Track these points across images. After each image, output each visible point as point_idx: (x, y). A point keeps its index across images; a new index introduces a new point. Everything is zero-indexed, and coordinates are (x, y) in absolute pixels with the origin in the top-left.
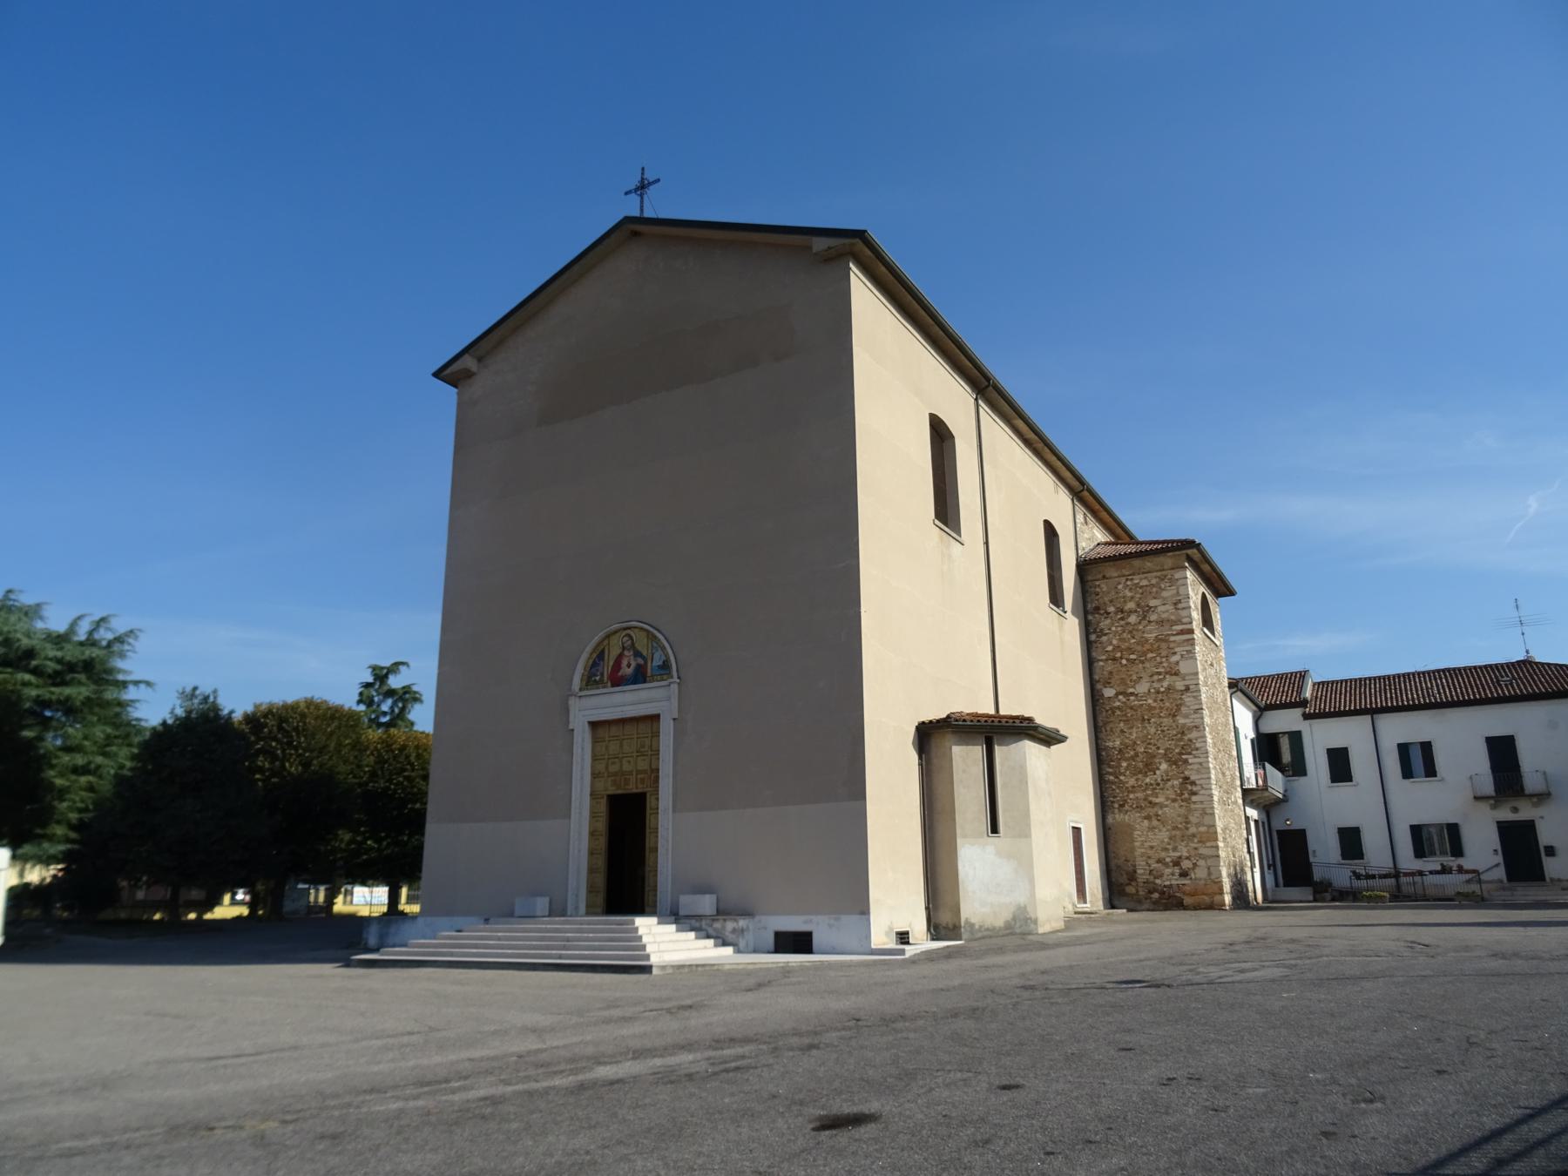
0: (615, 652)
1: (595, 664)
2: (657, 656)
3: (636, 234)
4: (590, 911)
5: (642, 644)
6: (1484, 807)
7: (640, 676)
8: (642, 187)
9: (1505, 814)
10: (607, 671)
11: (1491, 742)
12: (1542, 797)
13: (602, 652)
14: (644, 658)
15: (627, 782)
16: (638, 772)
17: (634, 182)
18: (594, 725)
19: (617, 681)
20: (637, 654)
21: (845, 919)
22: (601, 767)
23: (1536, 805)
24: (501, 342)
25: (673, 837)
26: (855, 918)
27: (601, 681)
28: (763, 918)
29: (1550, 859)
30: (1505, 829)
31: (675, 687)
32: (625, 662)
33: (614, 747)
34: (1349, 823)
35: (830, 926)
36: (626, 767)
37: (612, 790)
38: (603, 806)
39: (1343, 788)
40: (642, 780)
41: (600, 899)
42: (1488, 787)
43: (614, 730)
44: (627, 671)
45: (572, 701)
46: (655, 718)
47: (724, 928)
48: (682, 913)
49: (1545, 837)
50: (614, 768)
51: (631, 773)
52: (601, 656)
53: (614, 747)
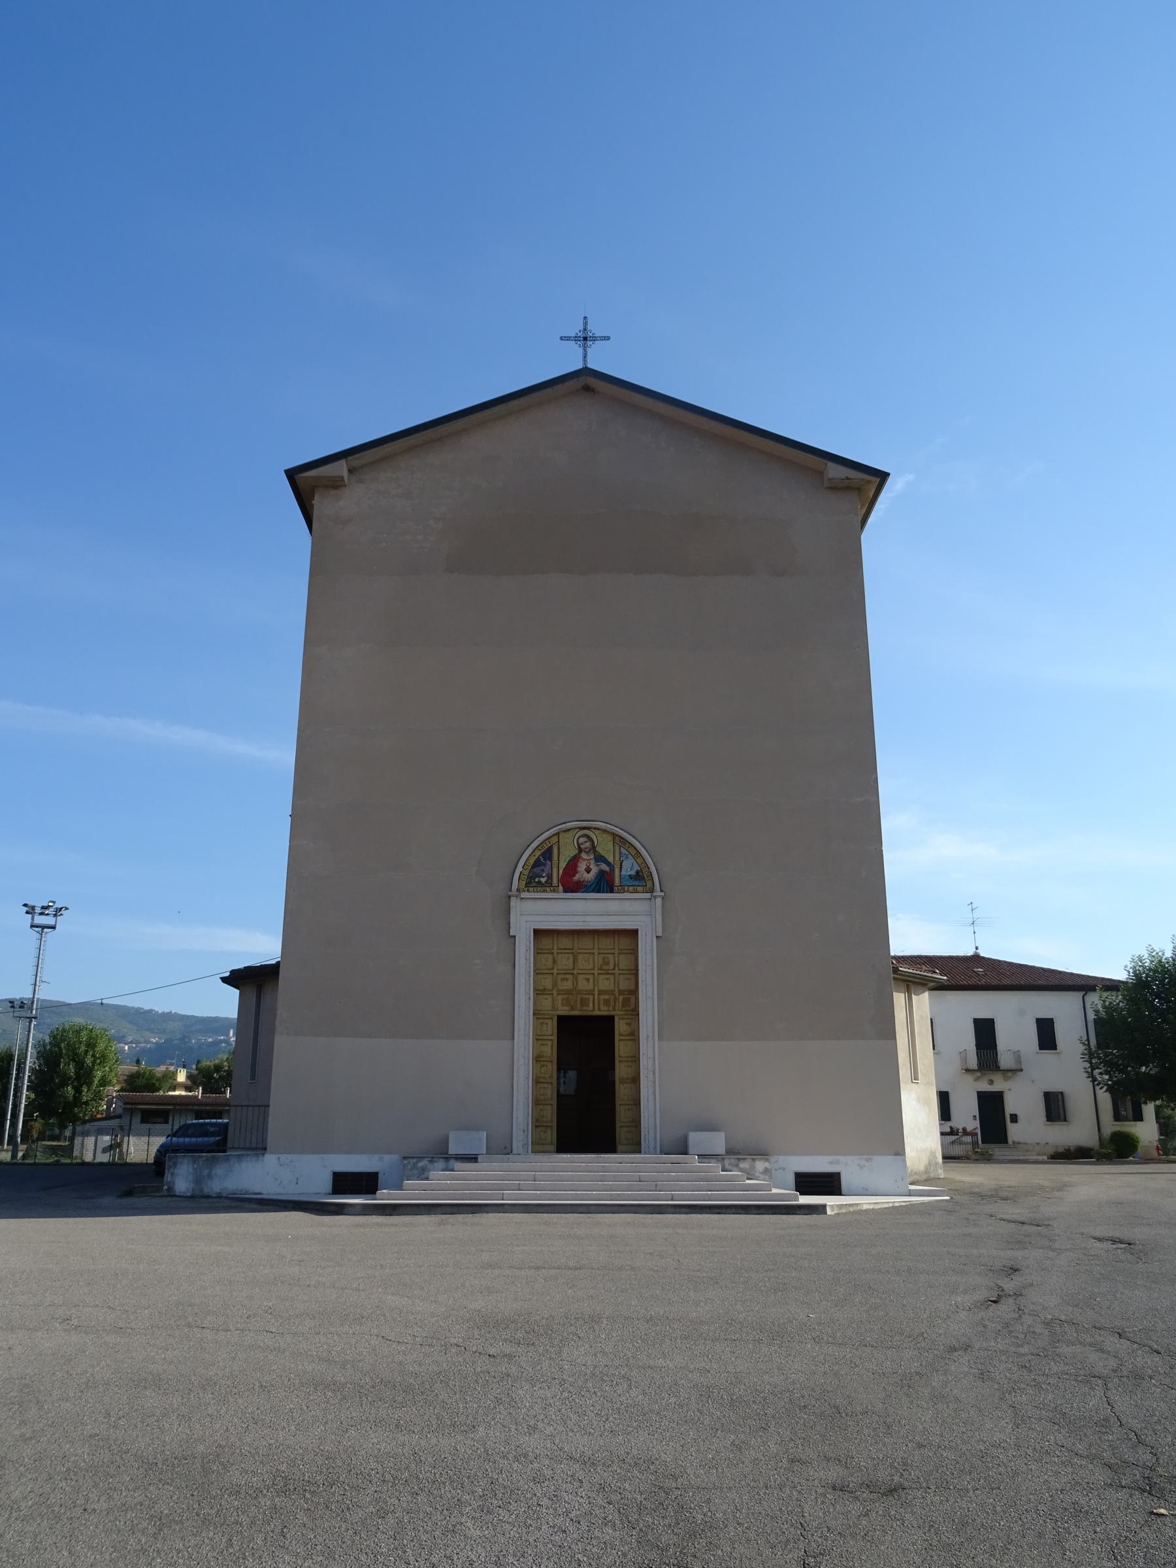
0: (568, 853)
1: (537, 863)
2: (627, 864)
3: (587, 389)
4: (538, 1147)
5: (606, 847)
6: (969, 1078)
7: (604, 884)
8: (585, 339)
9: (985, 1087)
10: (547, 872)
11: (977, 1022)
12: (1015, 1071)
13: (550, 850)
14: (608, 864)
15: (584, 1002)
16: (601, 992)
17: (576, 329)
18: (538, 933)
19: (571, 885)
20: (599, 859)
21: (879, 1160)
22: (547, 983)
23: (1006, 1079)
24: (386, 458)
25: (662, 1068)
26: (889, 1159)
27: (549, 882)
28: (781, 1158)
29: (1014, 1125)
30: (982, 1097)
31: (659, 901)
32: (582, 866)
33: (565, 962)
34: (1054, 1088)
35: (861, 1167)
36: (583, 985)
37: (564, 1011)
38: (551, 1028)
39: (1048, 1055)
40: (607, 1002)
41: (551, 1135)
42: (973, 1063)
43: (566, 942)
44: (582, 875)
45: (514, 902)
46: (635, 933)
47: (753, 1168)
48: (452, 1150)
49: (1010, 1107)
50: (568, 985)
51: (591, 992)
52: (548, 854)
53: (565, 962)
